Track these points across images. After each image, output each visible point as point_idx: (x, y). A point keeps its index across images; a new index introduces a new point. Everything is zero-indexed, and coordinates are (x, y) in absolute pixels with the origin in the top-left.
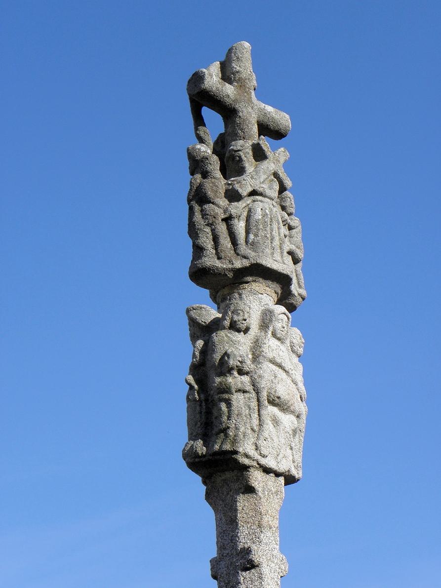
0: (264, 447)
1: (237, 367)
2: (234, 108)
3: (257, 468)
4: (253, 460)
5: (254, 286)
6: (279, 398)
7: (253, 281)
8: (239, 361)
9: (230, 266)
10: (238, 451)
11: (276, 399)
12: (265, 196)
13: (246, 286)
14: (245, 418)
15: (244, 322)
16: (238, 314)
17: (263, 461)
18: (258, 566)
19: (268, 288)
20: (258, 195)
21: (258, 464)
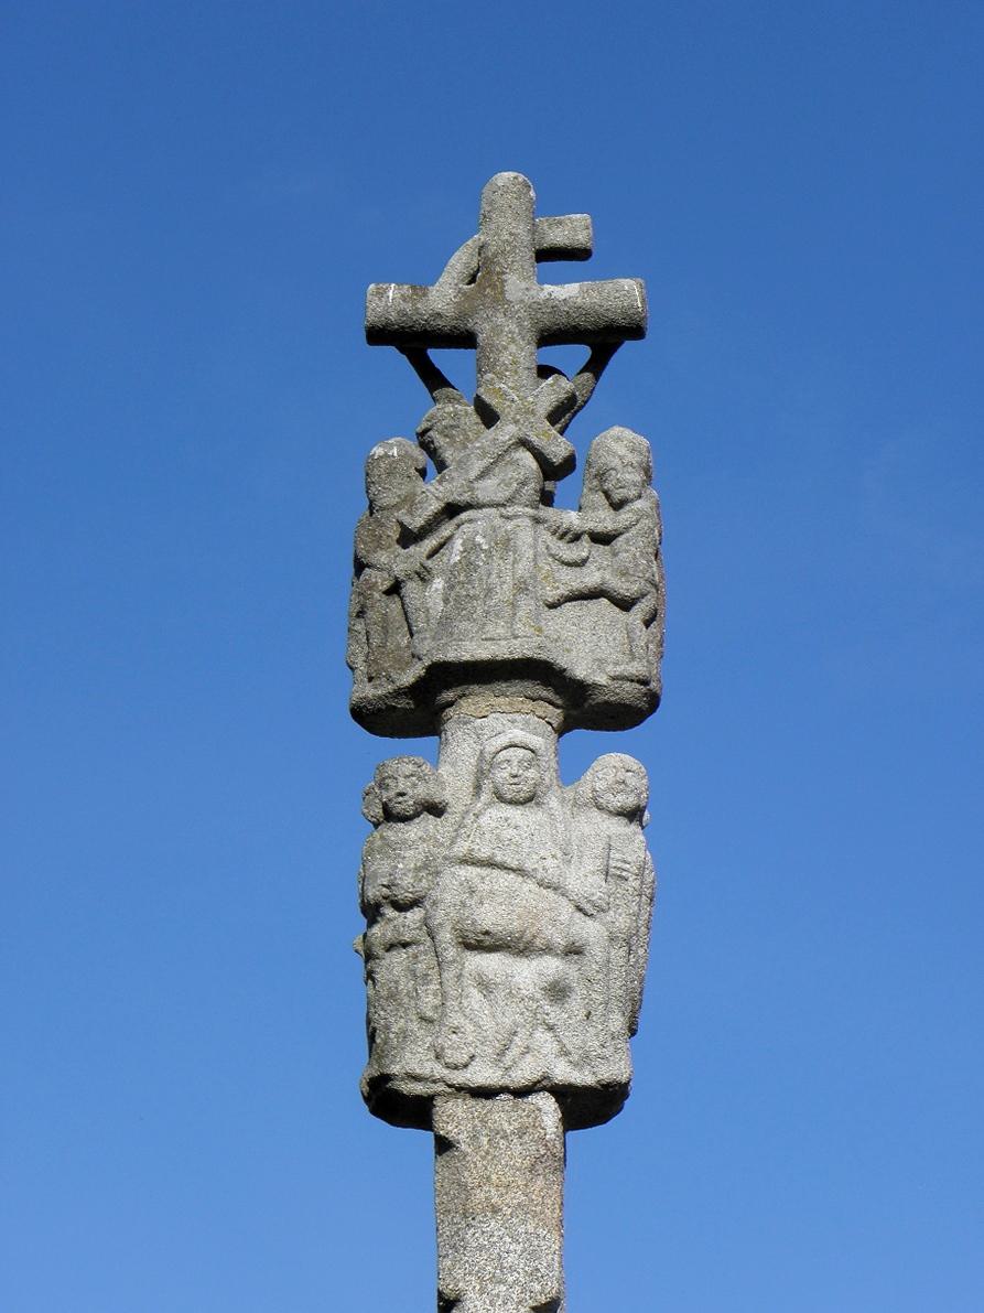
0: (450, 1047)
1: (384, 898)
2: (467, 331)
3: (449, 1094)
4: (434, 1082)
5: (466, 706)
6: (487, 933)
7: (460, 697)
8: (384, 886)
9: (390, 688)
10: (388, 1075)
11: (482, 937)
12: (480, 506)
13: (450, 711)
14: (406, 1000)
15: (401, 799)
16: (387, 787)
17: (459, 1078)
18: (459, 1301)
19: (501, 700)
20: (461, 512)
21: (450, 1086)
